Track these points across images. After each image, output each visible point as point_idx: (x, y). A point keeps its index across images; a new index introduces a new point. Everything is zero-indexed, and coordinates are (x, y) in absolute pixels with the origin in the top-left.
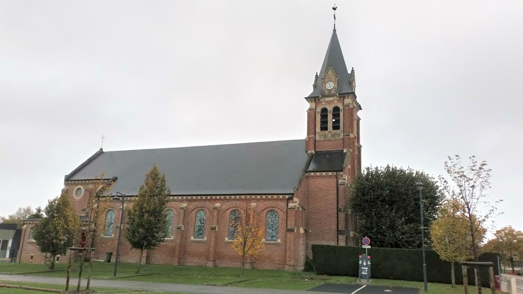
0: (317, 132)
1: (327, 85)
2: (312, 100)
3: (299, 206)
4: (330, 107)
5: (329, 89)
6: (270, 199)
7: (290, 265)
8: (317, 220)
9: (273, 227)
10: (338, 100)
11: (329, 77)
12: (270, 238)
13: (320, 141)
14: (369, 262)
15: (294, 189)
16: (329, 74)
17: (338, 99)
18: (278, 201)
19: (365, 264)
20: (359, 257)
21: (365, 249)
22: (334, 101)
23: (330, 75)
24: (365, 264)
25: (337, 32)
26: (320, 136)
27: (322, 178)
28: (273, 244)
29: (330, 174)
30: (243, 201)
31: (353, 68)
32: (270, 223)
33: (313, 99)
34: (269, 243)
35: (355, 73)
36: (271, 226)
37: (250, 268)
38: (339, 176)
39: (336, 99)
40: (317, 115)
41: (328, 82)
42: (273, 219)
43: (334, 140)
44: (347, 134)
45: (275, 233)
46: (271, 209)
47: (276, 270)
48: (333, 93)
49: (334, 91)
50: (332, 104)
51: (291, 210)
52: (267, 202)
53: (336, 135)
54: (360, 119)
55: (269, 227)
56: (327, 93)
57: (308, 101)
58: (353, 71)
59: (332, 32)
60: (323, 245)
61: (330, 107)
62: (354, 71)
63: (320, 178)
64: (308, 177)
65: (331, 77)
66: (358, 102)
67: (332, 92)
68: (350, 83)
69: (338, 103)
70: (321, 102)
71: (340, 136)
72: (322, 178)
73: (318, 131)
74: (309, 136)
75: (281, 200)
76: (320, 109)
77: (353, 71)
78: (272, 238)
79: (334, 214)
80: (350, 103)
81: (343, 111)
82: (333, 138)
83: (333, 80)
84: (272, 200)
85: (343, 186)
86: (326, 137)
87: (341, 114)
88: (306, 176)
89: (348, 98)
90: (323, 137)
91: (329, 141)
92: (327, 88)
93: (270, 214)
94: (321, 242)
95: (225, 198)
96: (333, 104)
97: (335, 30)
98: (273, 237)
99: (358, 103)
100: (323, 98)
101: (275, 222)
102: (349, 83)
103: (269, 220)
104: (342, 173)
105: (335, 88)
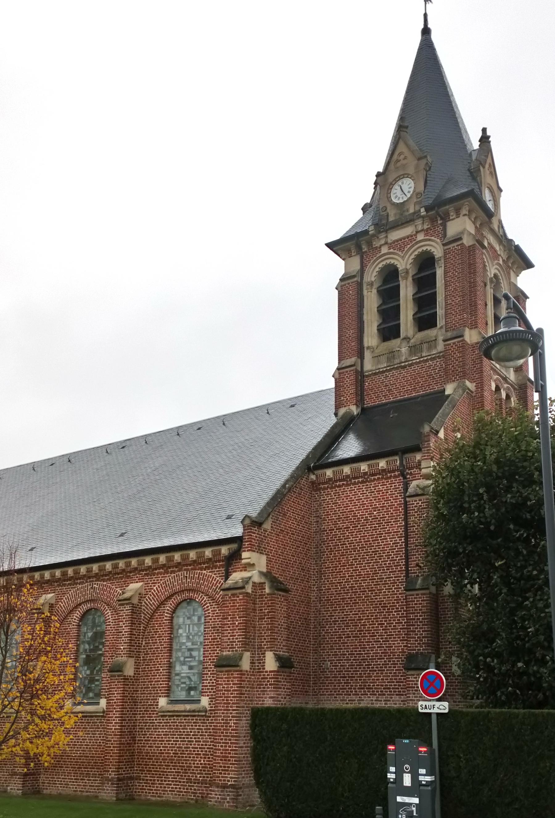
0: (368, 348)
1: (393, 191)
2: (349, 251)
3: (263, 580)
4: (403, 258)
5: (401, 201)
6: (179, 564)
7: (225, 787)
8: (347, 626)
9: (191, 656)
10: (426, 232)
11: (399, 164)
12: (182, 695)
13: (375, 374)
14: (422, 771)
15: (242, 522)
16: (400, 154)
17: (426, 227)
18: (201, 569)
19: (407, 780)
20: (385, 750)
21: (430, 714)
22: (416, 235)
23: (402, 157)
24: (407, 780)
25: (434, 37)
26: (377, 357)
27: (359, 482)
28: (187, 714)
29: (382, 464)
30: (109, 579)
31: (484, 130)
32: (184, 643)
33: (351, 245)
34: (177, 711)
35: (491, 143)
36: (187, 654)
37: (115, 799)
38: (412, 468)
39: (420, 228)
40: (365, 292)
41: (396, 180)
42: (193, 630)
43: (419, 363)
44: (455, 333)
45: (196, 676)
46: (186, 595)
47: (193, 802)
48: (412, 211)
49: (415, 204)
50: (409, 246)
51: (233, 595)
52: (173, 575)
53: (425, 346)
54: (527, 297)
55: (182, 659)
56: (395, 215)
57: (339, 255)
58: (485, 139)
59: (418, 38)
60: (283, 709)
61: (403, 258)
62: (490, 139)
63: (355, 483)
64: (319, 484)
65: (405, 162)
66: (510, 237)
67: (408, 210)
68: (471, 173)
69: (430, 240)
70: (376, 248)
71: (435, 347)
72: (359, 482)
73: (370, 345)
74: (342, 362)
75: (210, 563)
76: (375, 274)
77: (485, 139)
78: (189, 693)
79: (398, 600)
80: (465, 229)
81: (443, 261)
82: (415, 356)
83: (411, 170)
84: (187, 565)
85: (422, 497)
86: (394, 357)
87: (440, 272)
88: (313, 483)
89: (458, 216)
90: (384, 359)
91: (404, 367)
92: (396, 201)
93: (184, 613)
94: (360, 700)
95: (64, 574)
96: (413, 246)
97: (426, 31)
98: (190, 689)
99: (511, 240)
100: (383, 235)
101: (196, 638)
102: (468, 174)
103: (181, 634)
104: (418, 457)
105: (417, 194)
